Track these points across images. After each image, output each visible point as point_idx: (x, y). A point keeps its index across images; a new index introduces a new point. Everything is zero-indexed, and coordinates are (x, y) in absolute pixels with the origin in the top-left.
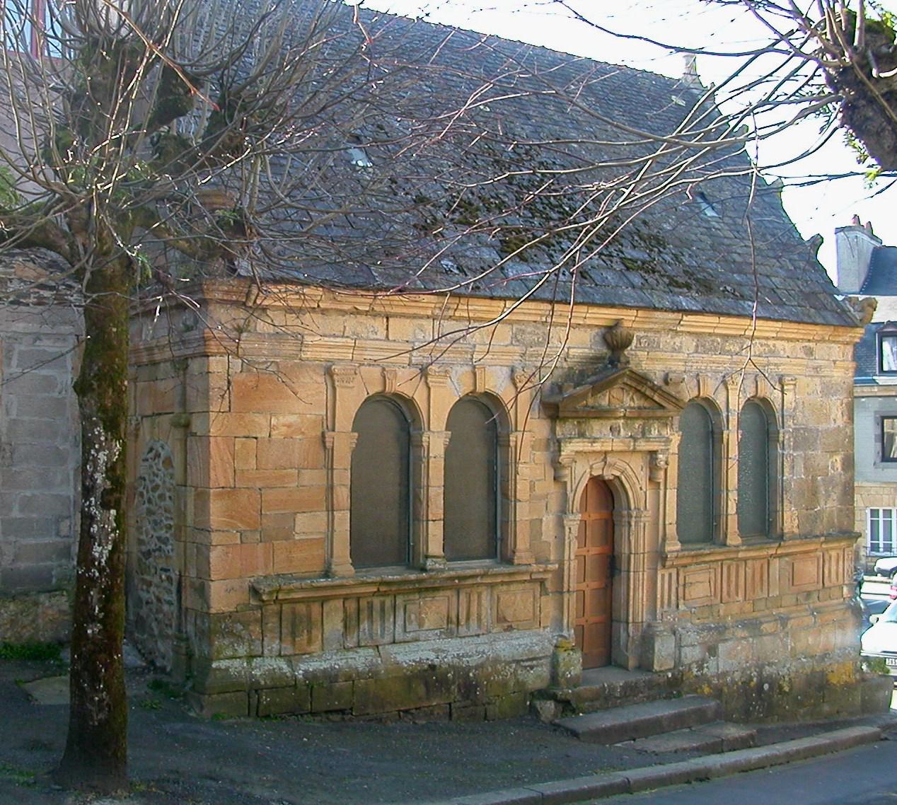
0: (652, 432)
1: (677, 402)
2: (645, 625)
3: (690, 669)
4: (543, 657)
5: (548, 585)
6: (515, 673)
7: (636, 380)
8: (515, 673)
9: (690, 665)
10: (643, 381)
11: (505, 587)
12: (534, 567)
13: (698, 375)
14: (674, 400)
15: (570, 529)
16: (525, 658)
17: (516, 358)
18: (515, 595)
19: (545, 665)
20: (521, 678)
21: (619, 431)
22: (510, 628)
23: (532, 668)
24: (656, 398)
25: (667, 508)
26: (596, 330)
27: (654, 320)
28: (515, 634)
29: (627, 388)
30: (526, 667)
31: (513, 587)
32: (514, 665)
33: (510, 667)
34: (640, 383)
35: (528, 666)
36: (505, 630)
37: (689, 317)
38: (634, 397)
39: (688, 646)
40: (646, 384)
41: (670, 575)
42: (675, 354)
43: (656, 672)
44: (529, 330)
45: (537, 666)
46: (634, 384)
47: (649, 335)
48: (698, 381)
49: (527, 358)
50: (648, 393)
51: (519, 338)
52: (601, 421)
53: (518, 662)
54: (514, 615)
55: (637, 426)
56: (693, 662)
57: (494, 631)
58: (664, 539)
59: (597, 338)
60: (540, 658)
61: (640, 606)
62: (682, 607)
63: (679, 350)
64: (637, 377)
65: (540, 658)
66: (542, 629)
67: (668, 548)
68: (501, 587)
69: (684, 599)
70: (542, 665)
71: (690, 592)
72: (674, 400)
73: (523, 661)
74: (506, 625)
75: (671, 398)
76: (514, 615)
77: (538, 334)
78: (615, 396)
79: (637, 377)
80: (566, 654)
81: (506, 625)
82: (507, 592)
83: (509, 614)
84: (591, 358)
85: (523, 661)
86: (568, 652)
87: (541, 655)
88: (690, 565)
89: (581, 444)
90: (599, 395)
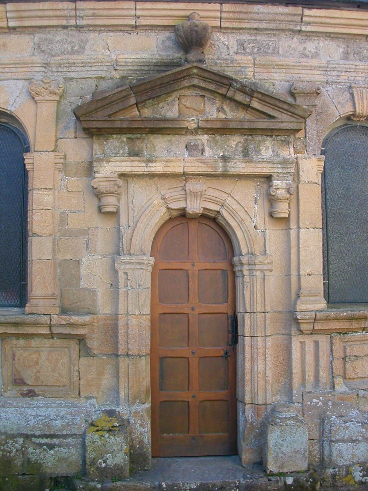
0: (263, 152)
1: (292, 110)
2: (269, 408)
3: (348, 473)
4: (71, 436)
5: (94, 344)
6: (23, 451)
7: (213, 81)
8: (23, 451)
9: (348, 467)
10: (226, 82)
11: (22, 342)
12: (55, 319)
13: (350, 87)
14: (285, 107)
15: (126, 273)
16: (38, 433)
17: (38, 69)
18: (38, 352)
19: (74, 446)
20: (33, 458)
21: (203, 151)
22: (31, 394)
23: (51, 447)
24: (255, 104)
25: (301, 253)
26: (167, 34)
27: (254, 16)
28: (39, 401)
29: (207, 94)
30: (41, 445)
31: (34, 342)
32: (21, 440)
33: (16, 442)
34: (221, 84)
35: (46, 444)
36: (24, 395)
37: (314, 10)
38: (225, 107)
39: (343, 441)
40: (230, 85)
41: (316, 343)
42: (304, 60)
43: (272, 474)
44: (58, 38)
45: (60, 446)
46: (212, 87)
47: (259, 38)
48: (352, 94)
49: (55, 69)
50: (239, 97)
51: (44, 48)
52: (169, 137)
53: (27, 437)
54: (37, 378)
55: (234, 144)
56: (354, 464)
57: (8, 394)
58: (298, 296)
59: (168, 43)
60: (65, 437)
61: (262, 382)
62: (341, 387)
63: (315, 55)
64: (213, 77)
65: (65, 437)
66: (82, 400)
67: (300, 306)
68: (15, 342)
69: (345, 378)
70: (68, 445)
71: (354, 368)
72: (285, 107)
73: (35, 436)
74: (25, 389)
75: (280, 105)
76: (37, 378)
77: (71, 42)
78: (188, 105)
79: (213, 77)
80: (96, 436)
81: (25, 389)
82: (27, 348)
83: (29, 377)
84: (156, 65)
85: (35, 436)
86: (100, 433)
87: (64, 433)
88: (354, 331)
89: (129, 164)
90: (161, 105)
